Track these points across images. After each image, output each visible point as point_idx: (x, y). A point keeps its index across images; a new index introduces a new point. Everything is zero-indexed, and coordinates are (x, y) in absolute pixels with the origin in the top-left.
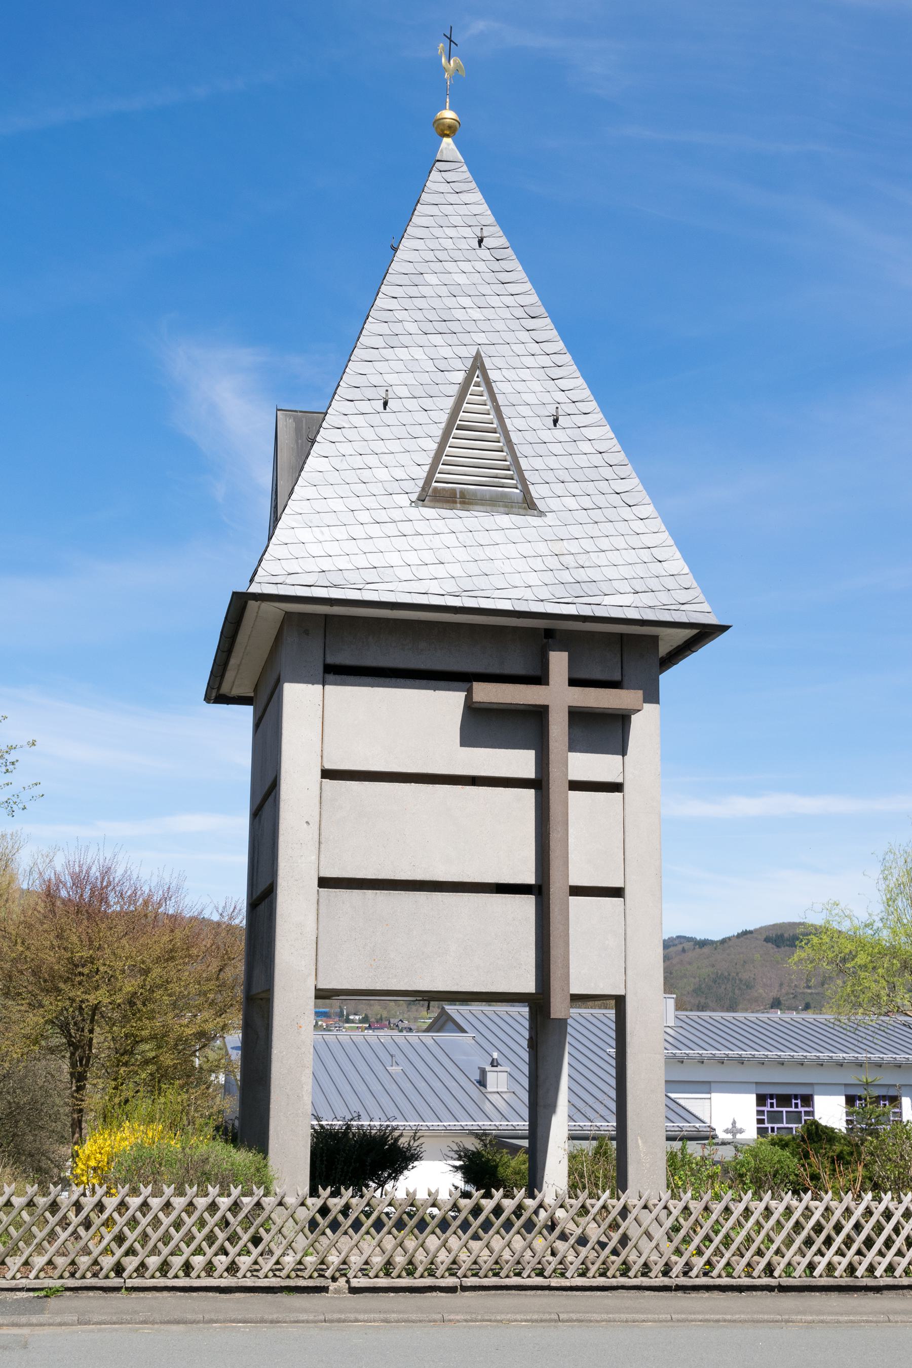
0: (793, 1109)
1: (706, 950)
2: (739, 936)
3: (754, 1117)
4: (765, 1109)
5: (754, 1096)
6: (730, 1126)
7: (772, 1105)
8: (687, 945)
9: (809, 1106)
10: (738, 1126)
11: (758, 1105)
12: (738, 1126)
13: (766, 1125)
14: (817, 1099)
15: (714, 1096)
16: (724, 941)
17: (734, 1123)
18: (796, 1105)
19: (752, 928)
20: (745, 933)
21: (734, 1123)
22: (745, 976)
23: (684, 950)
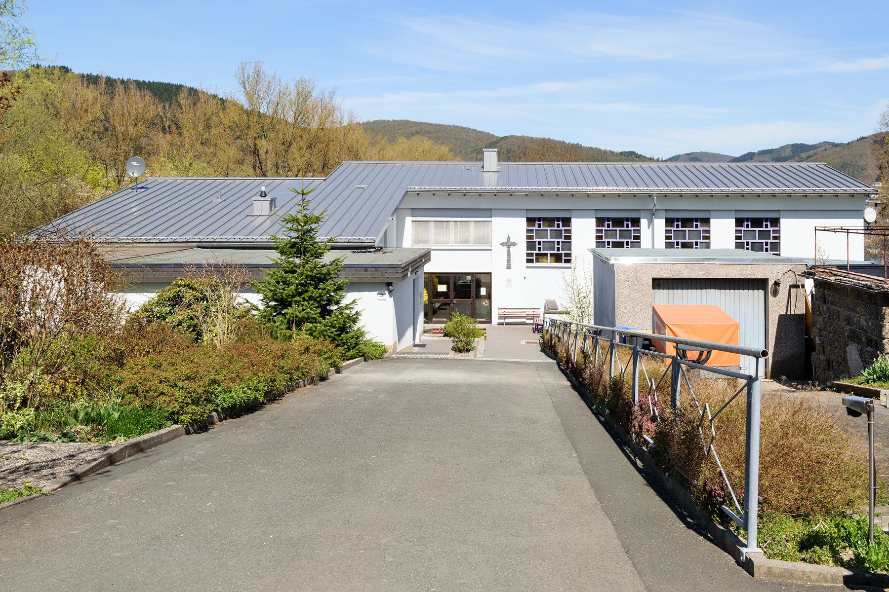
0: (764, 229)
1: (838, 149)
2: (858, 140)
3: (525, 234)
4: (604, 229)
5: (664, 220)
6: (505, 241)
7: (608, 226)
8: (828, 147)
9: (776, 226)
10: (512, 240)
11: (666, 226)
12: (512, 240)
13: (743, 241)
14: (783, 221)
15: (493, 219)
16: (849, 143)
17: (509, 238)
18: (627, 226)
19: (866, 136)
20: (862, 138)
21: (509, 238)
22: (861, 163)
23: (826, 150)
